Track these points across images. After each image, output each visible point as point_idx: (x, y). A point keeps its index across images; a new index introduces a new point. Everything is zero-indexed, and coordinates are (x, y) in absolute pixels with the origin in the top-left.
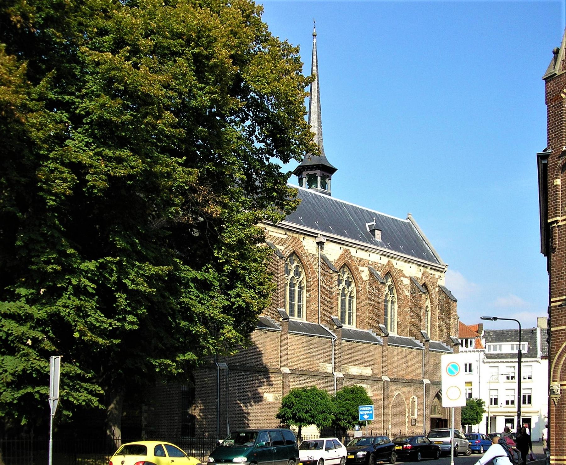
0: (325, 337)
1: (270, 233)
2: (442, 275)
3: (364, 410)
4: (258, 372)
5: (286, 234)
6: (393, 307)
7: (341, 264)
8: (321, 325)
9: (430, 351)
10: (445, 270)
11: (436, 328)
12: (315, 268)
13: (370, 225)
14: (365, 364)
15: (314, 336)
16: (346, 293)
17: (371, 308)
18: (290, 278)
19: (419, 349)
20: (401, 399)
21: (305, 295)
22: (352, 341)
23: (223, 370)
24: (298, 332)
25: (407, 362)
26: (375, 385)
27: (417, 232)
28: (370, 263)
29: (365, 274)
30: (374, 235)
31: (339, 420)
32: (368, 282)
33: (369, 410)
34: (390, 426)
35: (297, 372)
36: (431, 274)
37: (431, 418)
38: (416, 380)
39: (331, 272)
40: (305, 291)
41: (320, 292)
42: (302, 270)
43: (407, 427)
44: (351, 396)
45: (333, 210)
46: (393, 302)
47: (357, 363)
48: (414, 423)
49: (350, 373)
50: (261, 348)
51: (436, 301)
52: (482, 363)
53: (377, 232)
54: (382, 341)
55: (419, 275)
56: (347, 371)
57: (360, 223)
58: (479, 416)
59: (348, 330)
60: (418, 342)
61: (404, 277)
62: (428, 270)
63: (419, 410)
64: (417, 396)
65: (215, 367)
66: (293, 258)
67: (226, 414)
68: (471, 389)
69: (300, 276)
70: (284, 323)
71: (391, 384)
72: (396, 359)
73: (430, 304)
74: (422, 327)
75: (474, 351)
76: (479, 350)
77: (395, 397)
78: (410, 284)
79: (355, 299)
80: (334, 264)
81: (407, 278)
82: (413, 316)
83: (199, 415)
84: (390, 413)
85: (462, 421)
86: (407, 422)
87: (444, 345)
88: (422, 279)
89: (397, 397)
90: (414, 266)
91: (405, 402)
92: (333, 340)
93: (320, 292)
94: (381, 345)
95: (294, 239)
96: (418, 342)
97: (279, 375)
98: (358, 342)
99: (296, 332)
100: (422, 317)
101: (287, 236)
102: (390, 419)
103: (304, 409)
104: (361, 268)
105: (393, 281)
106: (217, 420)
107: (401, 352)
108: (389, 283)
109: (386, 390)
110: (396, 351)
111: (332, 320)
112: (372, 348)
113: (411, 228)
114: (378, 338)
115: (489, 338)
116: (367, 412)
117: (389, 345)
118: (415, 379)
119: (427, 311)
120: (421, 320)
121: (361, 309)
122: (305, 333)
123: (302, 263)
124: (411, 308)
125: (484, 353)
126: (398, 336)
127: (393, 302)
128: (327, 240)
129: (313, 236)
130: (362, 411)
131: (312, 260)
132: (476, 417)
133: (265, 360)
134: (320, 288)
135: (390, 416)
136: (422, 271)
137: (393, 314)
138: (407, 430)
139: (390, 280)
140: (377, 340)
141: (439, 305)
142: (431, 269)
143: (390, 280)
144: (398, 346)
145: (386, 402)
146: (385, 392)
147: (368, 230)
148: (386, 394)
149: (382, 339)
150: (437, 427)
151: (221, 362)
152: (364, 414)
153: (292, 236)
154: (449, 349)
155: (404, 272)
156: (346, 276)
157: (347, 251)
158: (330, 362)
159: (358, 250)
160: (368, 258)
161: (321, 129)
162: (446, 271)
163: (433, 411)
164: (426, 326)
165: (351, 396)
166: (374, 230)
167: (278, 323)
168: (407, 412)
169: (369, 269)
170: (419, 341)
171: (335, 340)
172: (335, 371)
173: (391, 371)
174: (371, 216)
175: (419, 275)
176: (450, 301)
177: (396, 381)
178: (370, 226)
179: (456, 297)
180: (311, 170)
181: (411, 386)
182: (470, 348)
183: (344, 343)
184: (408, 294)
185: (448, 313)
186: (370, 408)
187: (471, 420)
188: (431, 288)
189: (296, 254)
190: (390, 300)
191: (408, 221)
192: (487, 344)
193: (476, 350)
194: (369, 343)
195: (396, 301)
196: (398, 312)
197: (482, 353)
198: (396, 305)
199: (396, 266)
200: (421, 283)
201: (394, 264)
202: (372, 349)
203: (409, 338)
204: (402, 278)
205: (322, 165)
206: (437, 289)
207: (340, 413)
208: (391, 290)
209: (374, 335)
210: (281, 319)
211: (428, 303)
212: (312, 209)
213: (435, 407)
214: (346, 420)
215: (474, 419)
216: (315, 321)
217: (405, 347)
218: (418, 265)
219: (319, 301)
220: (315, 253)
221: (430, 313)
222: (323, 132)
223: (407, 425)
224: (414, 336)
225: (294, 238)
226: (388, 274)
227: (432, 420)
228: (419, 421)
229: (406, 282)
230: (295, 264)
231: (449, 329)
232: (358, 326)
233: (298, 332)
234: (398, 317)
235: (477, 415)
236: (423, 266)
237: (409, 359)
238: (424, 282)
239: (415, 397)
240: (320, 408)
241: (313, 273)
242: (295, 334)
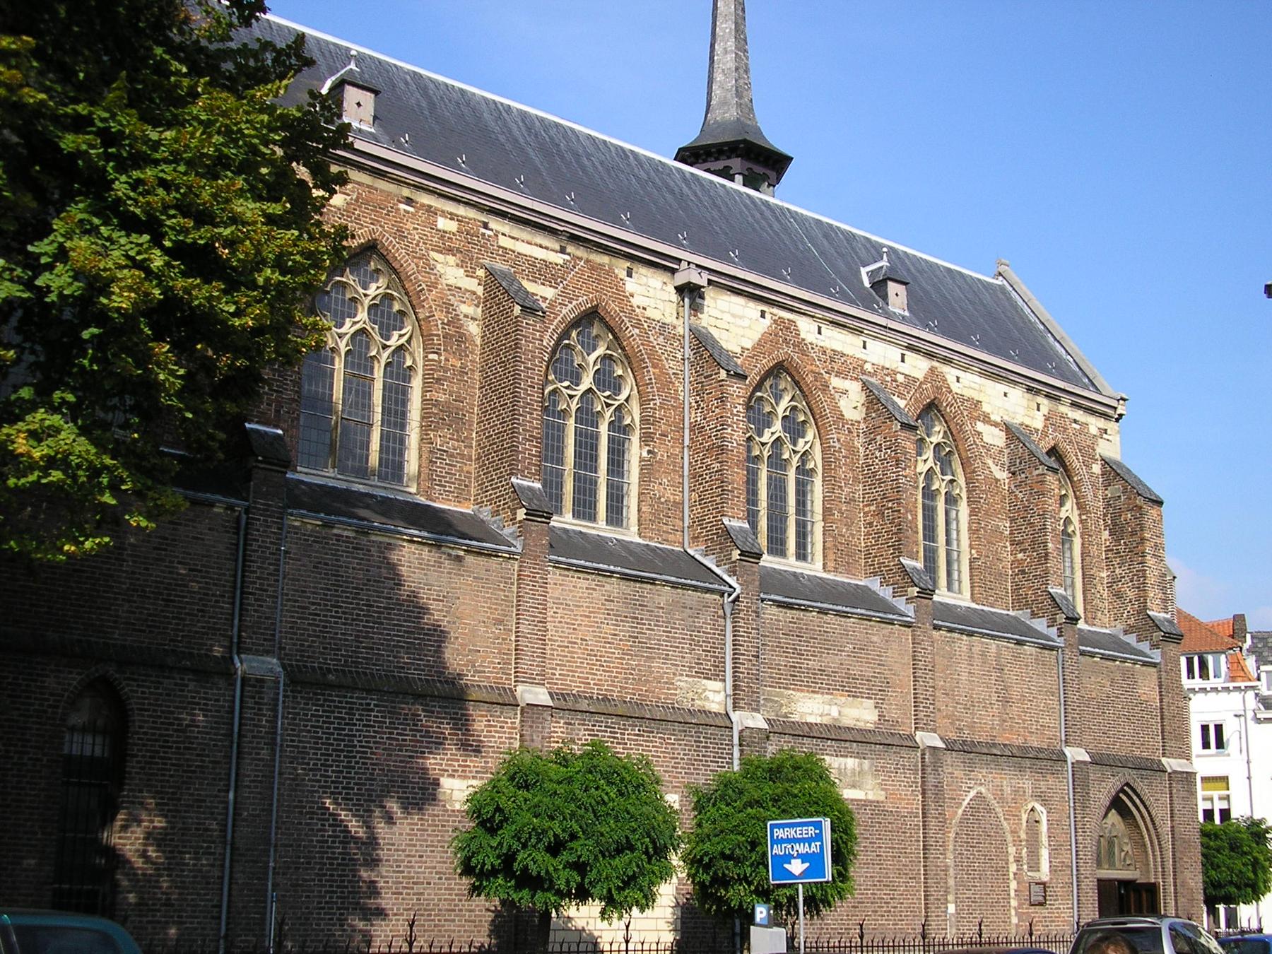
0: (696, 588)
1: (504, 241)
2: (1112, 426)
3: (788, 840)
4: (419, 697)
5: (563, 251)
6: (953, 514)
7: (766, 363)
8: (691, 552)
9: (1082, 653)
10: (1119, 412)
11: (1100, 587)
12: (672, 367)
13: (872, 271)
14: (851, 687)
15: (652, 582)
16: (786, 456)
17: (873, 508)
18: (579, 393)
19: (1044, 647)
20: (990, 810)
21: (635, 452)
22: (799, 608)
23: (261, 681)
24: (588, 564)
25: (1006, 689)
26: (891, 759)
27: (1027, 310)
28: (868, 367)
29: (851, 403)
30: (885, 297)
31: (725, 882)
32: (862, 426)
33: (809, 840)
34: (951, 908)
35: (584, 705)
36: (1075, 421)
37: (1099, 880)
38: (1040, 750)
39: (723, 374)
40: (635, 439)
41: (687, 442)
42: (625, 370)
43: (1013, 912)
44: (769, 789)
45: (750, 219)
46: (951, 500)
47: (820, 682)
48: (1040, 896)
49: (795, 718)
50: (437, 614)
51: (1097, 506)
52: (1251, 724)
53: (892, 287)
54: (911, 614)
55: (1038, 422)
56: (784, 710)
57: (841, 264)
58: (1260, 874)
59: (794, 574)
60: (1040, 625)
61: (984, 422)
62: (1064, 409)
63: (1054, 852)
64: (1044, 802)
65: (229, 674)
66: (595, 332)
67: (266, 852)
68: (1228, 798)
69: (617, 390)
70: (534, 527)
71: (949, 758)
72: (964, 676)
73: (1076, 512)
74: (1052, 578)
75: (1226, 689)
76: (1242, 685)
77: (965, 803)
78: (1008, 446)
79: (818, 480)
80: (739, 361)
81: (996, 425)
82: (1020, 543)
83: (144, 854)
84: (950, 862)
85: (1205, 890)
86: (1012, 894)
87: (1131, 639)
88: (1045, 434)
89: (974, 804)
90: (1017, 394)
91: (1005, 824)
92: (727, 600)
93: (687, 442)
94: (908, 625)
95: (592, 269)
96: (1040, 625)
97: (509, 711)
98: (824, 612)
99: (582, 562)
100: (1050, 545)
101: (567, 257)
102: (951, 882)
103: (544, 832)
104: (835, 382)
105: (949, 432)
106: (222, 878)
107: (983, 655)
108: (936, 439)
109: (931, 779)
110: (964, 648)
111: (727, 532)
112: (878, 634)
113: (1009, 299)
114: (900, 603)
115: (1265, 654)
116: (801, 848)
117: (936, 628)
118: (1035, 744)
119: (1069, 535)
120: (1047, 554)
121: (840, 511)
122: (619, 569)
123: (623, 349)
124: (1013, 520)
125: (1257, 695)
126: (974, 606)
127: (951, 500)
128: (709, 281)
129: (665, 265)
130: (780, 841)
131: (661, 339)
132: (1251, 875)
133: (454, 658)
134: (687, 431)
135: (951, 872)
136: (1044, 410)
137: (954, 535)
138: (1015, 920)
139: (939, 428)
140: (893, 610)
141: (1105, 515)
142: (1074, 404)
143: (939, 428)
144: (970, 634)
145: (932, 823)
146: (929, 786)
147: (867, 284)
148: (932, 795)
149: (911, 607)
150: (1124, 910)
151: (257, 653)
152: (788, 858)
153: (587, 261)
154: (1147, 651)
155: (986, 408)
156: (785, 403)
157: (789, 327)
158: (718, 675)
159: (824, 328)
160: (860, 353)
161: (747, 59)
162: (1121, 415)
163: (1105, 853)
164: (1069, 581)
165: (769, 789)
166: (884, 281)
167: (513, 528)
168: (1011, 859)
169: (866, 386)
170: (1044, 621)
171: (737, 598)
172: (735, 707)
173: (947, 717)
174: (875, 251)
175: (1038, 422)
176: (1139, 501)
177: (966, 749)
178: (871, 274)
179: (1159, 491)
180: (717, 159)
181: (1021, 769)
182: (1213, 682)
183: (771, 612)
184: (1002, 475)
185: (1136, 538)
186: (812, 831)
187: (1238, 888)
188: (1076, 464)
189: (602, 319)
190: (943, 491)
191: (1000, 281)
192: (1263, 668)
193: (1231, 685)
194: (863, 618)
195: (964, 495)
196: (970, 529)
197: (1251, 694)
198: (964, 508)
199: (955, 388)
200: (1046, 445)
201: (951, 379)
202: (875, 639)
203: (1011, 613)
204: (980, 426)
205: (745, 141)
206: (1097, 468)
207: (724, 857)
208: (944, 460)
209: (886, 593)
210: (521, 514)
211: (1070, 509)
212: (675, 205)
213: (1111, 843)
214: (750, 883)
215: (1247, 885)
216: (671, 537)
217: (993, 637)
218: (1030, 389)
219: (686, 473)
220: (670, 319)
221: (1077, 541)
222: (750, 67)
223: (1014, 903)
224: (1027, 605)
225: (594, 267)
226: (931, 409)
227: (1103, 885)
228: (1057, 889)
229: (994, 437)
230: (601, 351)
231: (1141, 588)
232: (831, 564)
233: (588, 564)
234: (971, 547)
235: (1255, 872)
236: (1048, 396)
237: (1011, 676)
238: (1052, 443)
239: (1038, 807)
240: (610, 830)
241: (665, 383)
242: (579, 569)
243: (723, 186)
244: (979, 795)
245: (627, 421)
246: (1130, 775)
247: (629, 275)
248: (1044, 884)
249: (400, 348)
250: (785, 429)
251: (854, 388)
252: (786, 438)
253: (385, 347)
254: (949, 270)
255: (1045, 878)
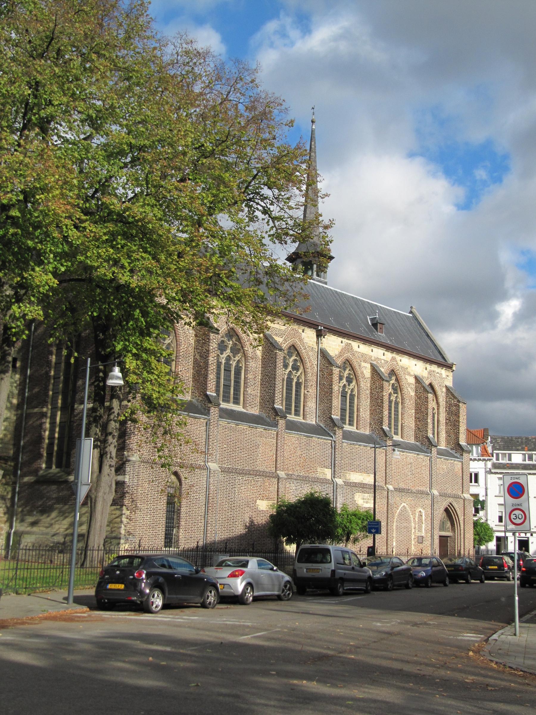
48: (420, 540)
57: (361, 315)
76: (486, 458)
86: (413, 539)
98: (360, 445)
105: (397, 380)
139: (394, 378)
168: (413, 528)
192: (495, 452)
193: (482, 458)
200: (427, 382)
204: (407, 377)
226: (393, 372)
229: (412, 380)
239: (421, 510)
243: (323, 287)
244: (404, 506)
245: (301, 381)
246: (450, 500)
247: (303, 332)
248: (423, 536)
249: (239, 360)
250: (347, 381)
251: (369, 366)
252: (347, 384)
253: (234, 360)
254: (395, 312)
255: (423, 535)
